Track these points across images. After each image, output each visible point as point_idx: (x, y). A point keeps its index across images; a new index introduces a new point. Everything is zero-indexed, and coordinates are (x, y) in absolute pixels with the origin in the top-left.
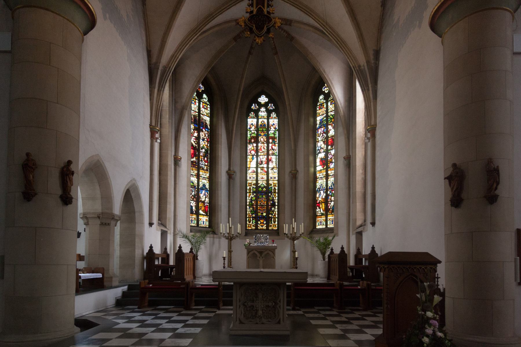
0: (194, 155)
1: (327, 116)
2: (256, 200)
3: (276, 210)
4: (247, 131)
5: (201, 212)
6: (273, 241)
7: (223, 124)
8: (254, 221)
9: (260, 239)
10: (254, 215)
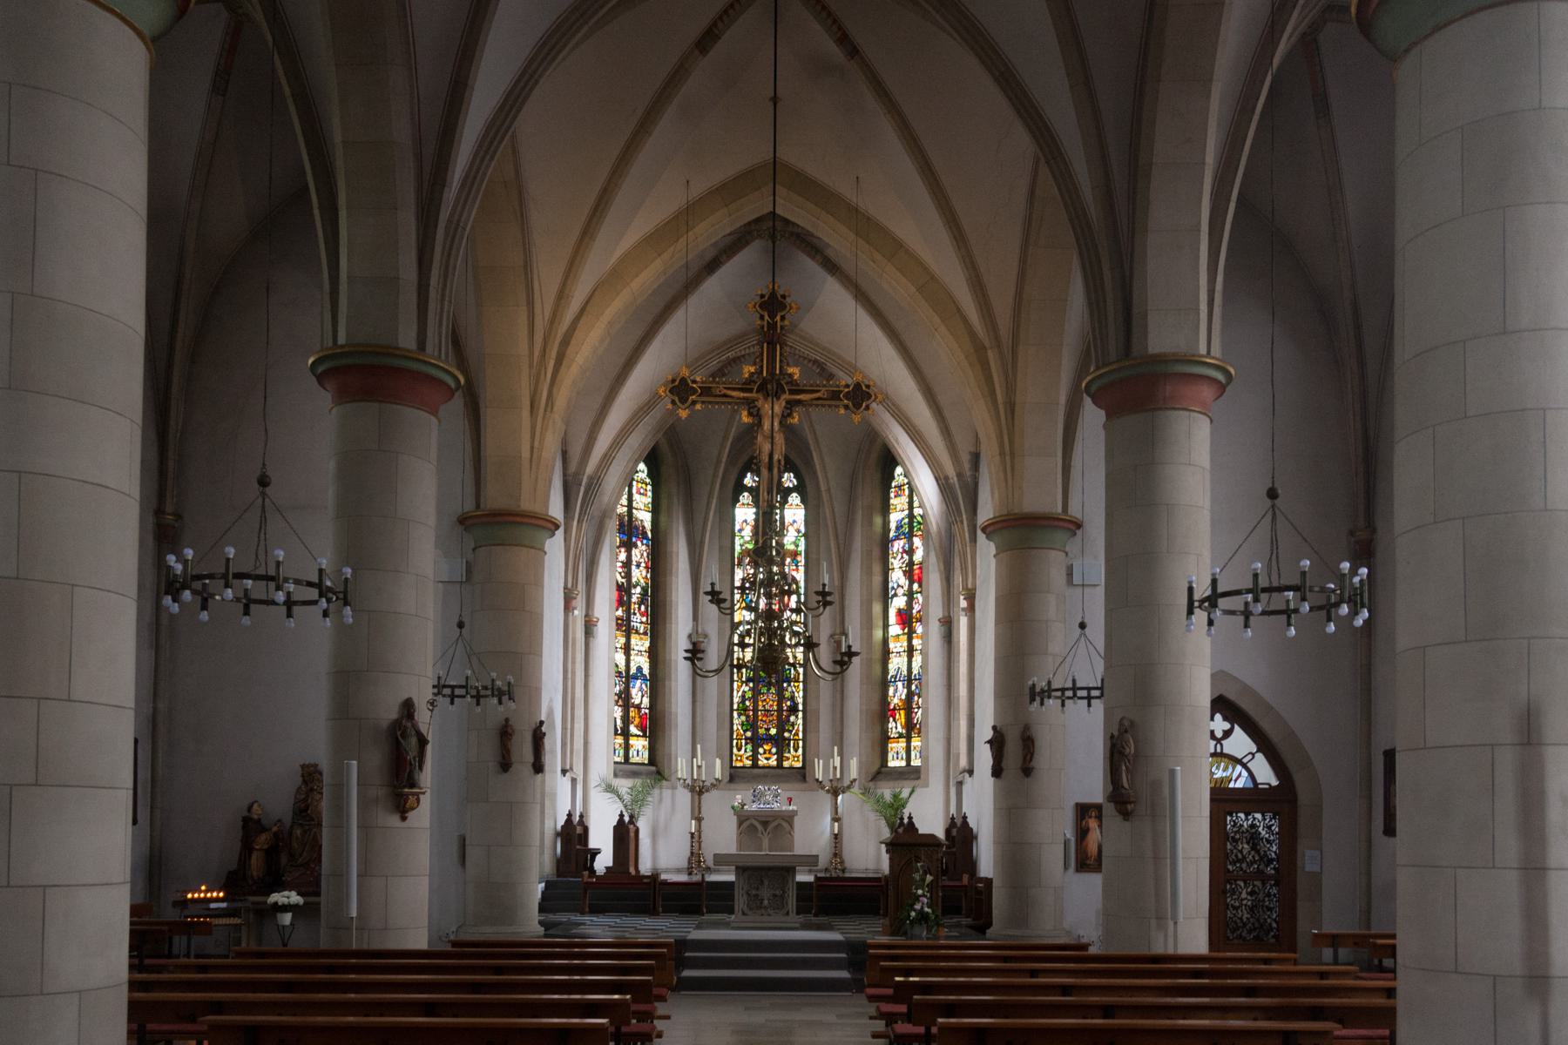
0: (620, 603)
1: (911, 516)
2: (755, 699)
3: (800, 721)
4: (733, 536)
5: (633, 729)
6: (790, 800)
7: (681, 530)
8: (749, 747)
9: (762, 794)
10: (749, 734)
